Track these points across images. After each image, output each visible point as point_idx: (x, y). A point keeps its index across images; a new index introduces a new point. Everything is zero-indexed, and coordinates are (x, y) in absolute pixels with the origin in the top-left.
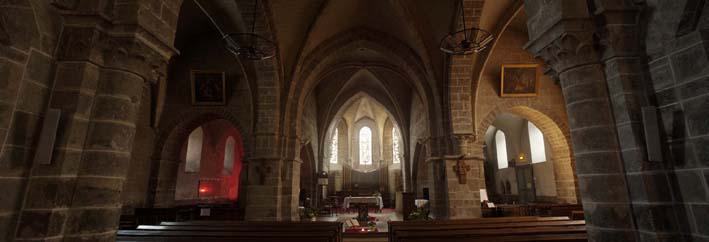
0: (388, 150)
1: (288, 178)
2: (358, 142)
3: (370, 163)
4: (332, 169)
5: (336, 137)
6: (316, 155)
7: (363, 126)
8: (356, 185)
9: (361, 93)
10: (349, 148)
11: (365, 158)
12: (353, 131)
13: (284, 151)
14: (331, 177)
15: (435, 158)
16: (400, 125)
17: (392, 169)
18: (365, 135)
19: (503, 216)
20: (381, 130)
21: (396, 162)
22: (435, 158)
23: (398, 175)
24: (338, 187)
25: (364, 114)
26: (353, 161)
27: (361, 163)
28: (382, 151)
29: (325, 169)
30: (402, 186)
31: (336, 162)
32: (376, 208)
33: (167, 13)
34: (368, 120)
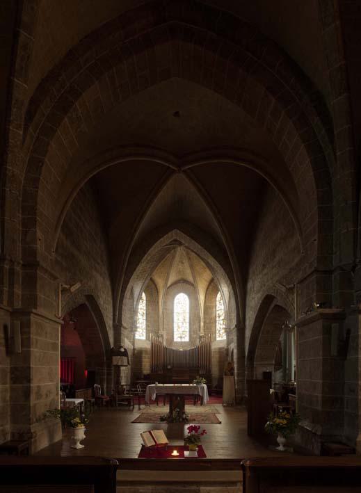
0: (210, 322)
1: (19, 349)
2: (172, 313)
3: (187, 339)
4: (138, 346)
5: (142, 307)
6: (109, 322)
7: (178, 293)
8: (169, 367)
9: (174, 234)
10: (159, 320)
11: (181, 333)
12: (165, 303)
13: (11, 295)
14: (138, 355)
15: (327, 311)
16: (232, 283)
17: (214, 347)
18: (181, 304)
19: (222, 388)
20: (202, 297)
21: (221, 336)
22: (327, 311)
23: (224, 354)
24: (146, 367)
25: (180, 277)
26: (165, 337)
27: (176, 339)
28: (202, 324)
29: (127, 344)
30: (233, 369)
31: (144, 338)
32: (197, 399)
33: (125, 328)
34: (185, 284)
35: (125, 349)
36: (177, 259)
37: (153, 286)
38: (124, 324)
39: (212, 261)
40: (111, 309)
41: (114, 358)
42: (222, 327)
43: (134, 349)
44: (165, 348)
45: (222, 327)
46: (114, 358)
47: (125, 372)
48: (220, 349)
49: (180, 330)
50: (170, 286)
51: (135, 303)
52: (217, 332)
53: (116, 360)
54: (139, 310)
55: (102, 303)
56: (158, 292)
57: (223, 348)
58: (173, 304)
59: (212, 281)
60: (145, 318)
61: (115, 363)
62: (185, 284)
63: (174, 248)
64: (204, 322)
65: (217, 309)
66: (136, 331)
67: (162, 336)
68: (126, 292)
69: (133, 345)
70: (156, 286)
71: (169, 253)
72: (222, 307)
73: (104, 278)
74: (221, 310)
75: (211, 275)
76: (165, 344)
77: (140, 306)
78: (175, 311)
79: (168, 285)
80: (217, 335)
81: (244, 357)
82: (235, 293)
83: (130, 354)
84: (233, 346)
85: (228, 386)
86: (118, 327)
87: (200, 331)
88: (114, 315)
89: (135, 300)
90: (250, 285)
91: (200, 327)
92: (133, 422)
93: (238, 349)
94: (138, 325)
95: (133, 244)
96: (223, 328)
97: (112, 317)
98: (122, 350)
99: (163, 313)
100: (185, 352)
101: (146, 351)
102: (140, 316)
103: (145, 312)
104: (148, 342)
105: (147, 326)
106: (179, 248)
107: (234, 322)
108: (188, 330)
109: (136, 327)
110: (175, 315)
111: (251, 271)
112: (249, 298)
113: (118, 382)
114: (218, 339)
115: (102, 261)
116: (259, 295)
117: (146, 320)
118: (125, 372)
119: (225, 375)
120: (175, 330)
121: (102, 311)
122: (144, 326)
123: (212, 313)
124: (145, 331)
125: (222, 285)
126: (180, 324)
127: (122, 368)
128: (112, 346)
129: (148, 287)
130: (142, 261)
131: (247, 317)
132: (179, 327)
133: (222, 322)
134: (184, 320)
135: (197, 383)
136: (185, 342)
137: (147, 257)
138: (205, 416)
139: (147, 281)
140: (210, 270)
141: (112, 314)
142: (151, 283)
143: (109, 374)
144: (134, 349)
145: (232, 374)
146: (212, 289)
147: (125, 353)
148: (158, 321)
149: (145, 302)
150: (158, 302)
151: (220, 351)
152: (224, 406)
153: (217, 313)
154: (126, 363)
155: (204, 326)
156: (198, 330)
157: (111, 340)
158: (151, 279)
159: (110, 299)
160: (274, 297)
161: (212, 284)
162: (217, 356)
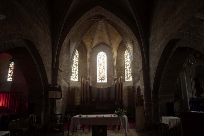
3: (105, 81)
5: (76, 60)
6: (48, 65)
8: (93, 100)
12: (91, 58)
14: (72, 91)
17: (125, 86)
20: (115, 53)
23: (132, 90)
26: (91, 80)
27: (99, 81)
28: (116, 71)
29: (63, 83)
30: (142, 101)
33: (62, 71)
35: (59, 86)
36: (99, 28)
38: (61, 68)
39: (123, 25)
41: (50, 92)
42: (128, 72)
43: (69, 87)
44: (90, 87)
45: (128, 72)
46: (50, 92)
47: (60, 104)
48: (128, 87)
49: (101, 75)
50: (94, 47)
51: (71, 56)
52: (126, 76)
53: (52, 94)
54: (74, 62)
55: (42, 49)
56: (86, 51)
57: (131, 86)
58: (96, 58)
60: (78, 67)
61: (50, 97)
64: (117, 70)
65: (125, 61)
66: (71, 75)
67: (89, 79)
69: (69, 85)
70: (85, 47)
72: (129, 60)
74: (128, 61)
77: (74, 59)
78: (98, 63)
80: (126, 78)
81: (150, 91)
84: (140, 84)
85: (139, 113)
86: (55, 70)
87: (114, 75)
88: (53, 61)
89: (71, 54)
90: (151, 39)
91: (114, 73)
96: (130, 73)
97: (51, 62)
99: (90, 64)
100: (104, 89)
103: (78, 63)
104: (79, 83)
105: (79, 72)
106: (100, 21)
107: (141, 66)
108: (106, 75)
109: (71, 73)
110: (98, 65)
112: (151, 47)
113: (53, 113)
114: (127, 80)
117: (79, 68)
118: (60, 104)
119: (137, 105)
120: (98, 75)
122: (77, 73)
124: (77, 75)
125: (128, 45)
126: (101, 71)
127: (57, 101)
132: (100, 73)
133: (128, 69)
134: (104, 68)
135: (119, 114)
136: (105, 83)
137: (78, 24)
141: (51, 60)
144: (69, 87)
145: (142, 105)
146: (122, 48)
147: (59, 89)
148: (86, 69)
150: (86, 57)
151: (129, 88)
152: (137, 131)
153: (125, 63)
154: (59, 97)
155: (117, 72)
156: (113, 74)
157: (50, 79)
158: (82, 42)
162: (127, 92)
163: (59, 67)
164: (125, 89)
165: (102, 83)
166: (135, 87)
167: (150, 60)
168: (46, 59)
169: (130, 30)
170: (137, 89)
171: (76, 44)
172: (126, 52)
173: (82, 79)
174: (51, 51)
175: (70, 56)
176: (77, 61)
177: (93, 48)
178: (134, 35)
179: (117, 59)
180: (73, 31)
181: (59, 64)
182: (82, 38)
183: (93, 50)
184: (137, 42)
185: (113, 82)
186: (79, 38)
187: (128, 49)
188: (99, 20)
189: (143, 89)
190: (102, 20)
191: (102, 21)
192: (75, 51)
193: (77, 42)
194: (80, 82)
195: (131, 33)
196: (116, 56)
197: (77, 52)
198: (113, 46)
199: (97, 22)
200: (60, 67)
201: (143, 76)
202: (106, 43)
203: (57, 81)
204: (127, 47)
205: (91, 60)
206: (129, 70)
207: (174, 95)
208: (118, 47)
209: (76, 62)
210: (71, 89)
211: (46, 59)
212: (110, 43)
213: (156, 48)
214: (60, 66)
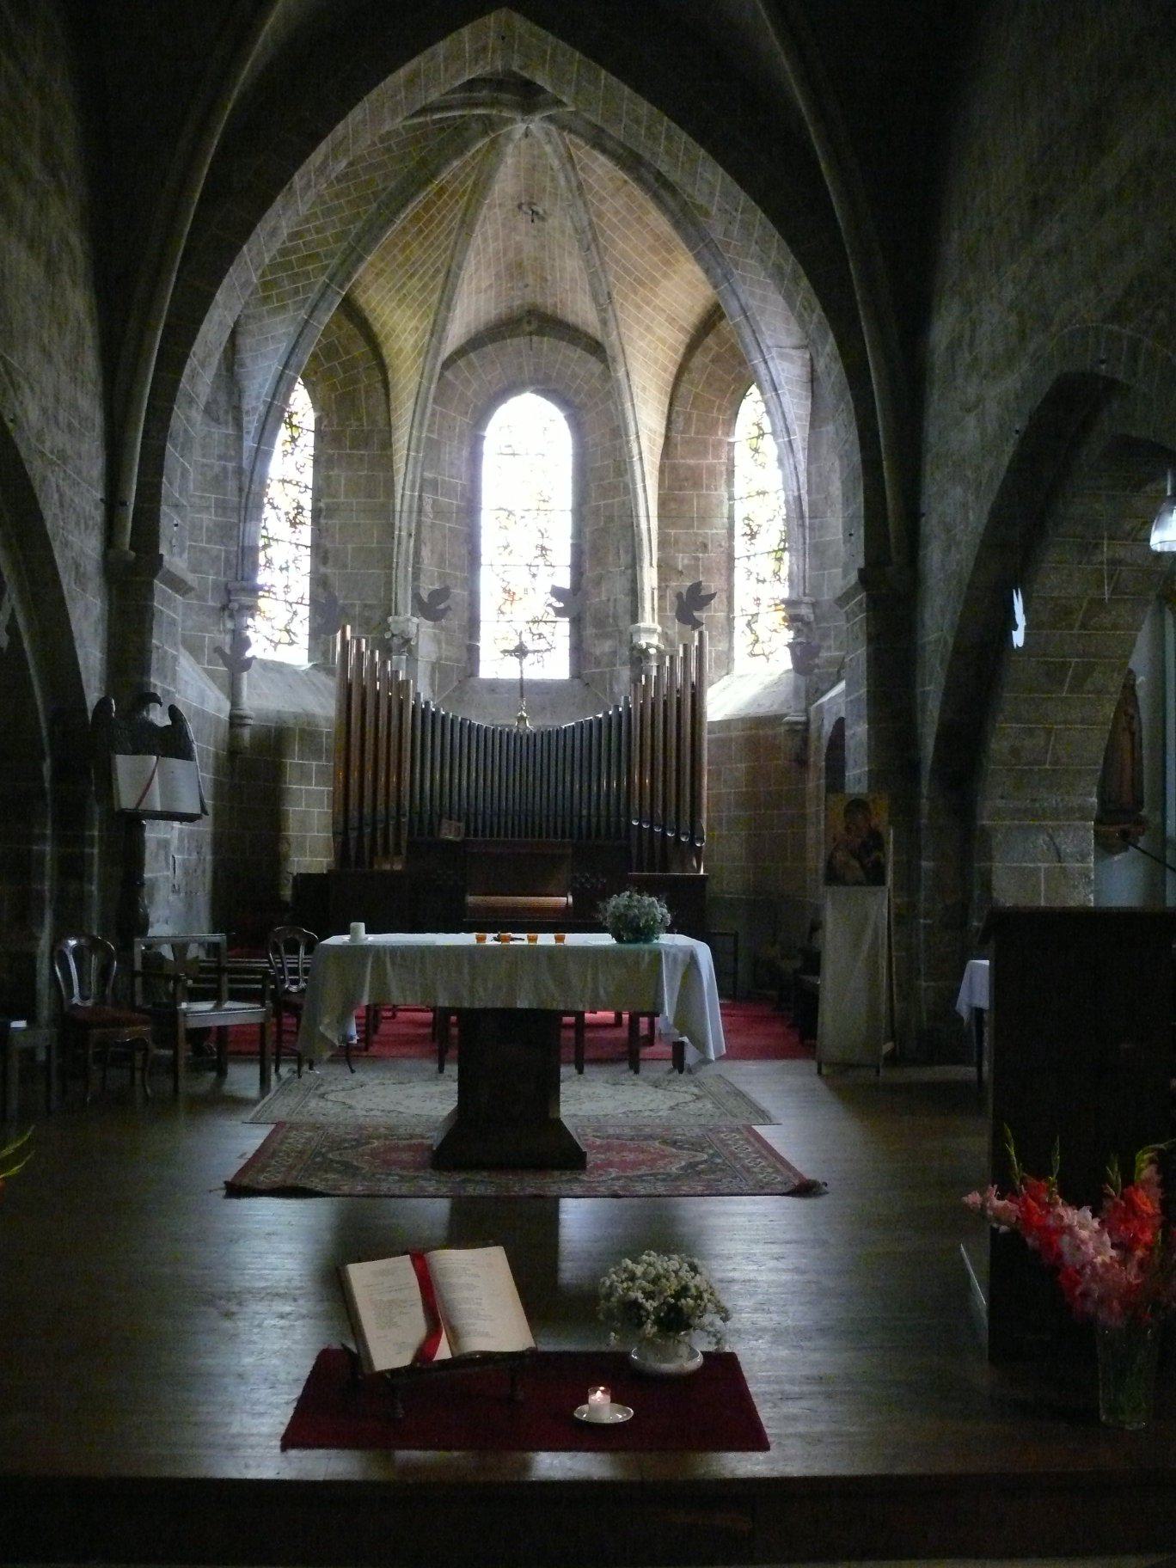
4: (261, 700)
25: (518, 300)
27: (493, 666)
31: (298, 656)
33: (178, 585)
35: (174, 712)
36: (506, 182)
37: (360, 349)
40: (94, 467)
41: (124, 764)
44: (425, 716)
50: (460, 352)
51: (249, 443)
52: (740, 623)
55: (33, 414)
59: (711, 320)
60: (305, 534)
62: (546, 343)
63: (489, 125)
65: (739, 490)
66: (252, 610)
68: (192, 362)
69: (234, 695)
71: (460, 152)
73: (51, 269)
75: (708, 291)
76: (423, 690)
79: (448, 348)
82: (856, 376)
83: (205, 743)
87: (635, 616)
88: (112, 502)
89: (251, 423)
90: (942, 330)
92: (236, 1190)
93: (873, 721)
94: (262, 578)
95: (245, 73)
97: (98, 515)
98: (158, 717)
101: (308, 734)
102: (273, 523)
103: (307, 501)
104: (322, 678)
106: (519, 128)
109: (254, 591)
111: (953, 245)
112: (939, 405)
115: (53, 170)
116: (1011, 382)
121: (35, 468)
123: (704, 518)
124: (304, 612)
127: (155, 833)
128: (93, 697)
129: (328, 351)
130: (298, 180)
131: (931, 525)
133: (766, 566)
138: (696, 1146)
139: (325, 317)
140: (699, 258)
141: (99, 494)
142: (349, 327)
143: (71, 868)
144: (236, 721)
147: (174, 742)
149: (308, 440)
150: (387, 444)
156: (624, 600)
157: (91, 656)
158: (351, 310)
159: (90, 406)
160: (1111, 384)
161: (710, 341)
163: (163, 550)
164: (722, 744)
165: (522, 688)
166: (813, 727)
167: (924, 509)
168: (61, 496)
169: (777, 235)
170: (825, 742)
171: (292, 330)
172: (752, 407)
173: (345, 644)
174: (98, 418)
175: (239, 438)
176: (295, 476)
177: (449, 363)
178: (805, 282)
179: (662, 471)
180: (274, 232)
181: (164, 522)
182: (348, 277)
183: (449, 375)
184: (828, 349)
185: (625, 673)
186: (324, 279)
187: (767, 386)
188: (506, 114)
189: (864, 750)
190: (537, 117)
191: (536, 124)
192: (290, 389)
193: (303, 315)
194: (330, 672)
195: (788, 269)
196: (660, 441)
197: (301, 401)
198: (628, 349)
199: (485, 133)
200: (171, 553)
201: (863, 638)
202: (571, 318)
203: (144, 669)
204: (762, 369)
205: (428, 475)
206: (767, 574)
207: (1094, 800)
208: (678, 358)
209: (293, 491)
210: (246, 733)
211: (61, 496)
212: (604, 302)
213: (971, 421)
214: (172, 546)
